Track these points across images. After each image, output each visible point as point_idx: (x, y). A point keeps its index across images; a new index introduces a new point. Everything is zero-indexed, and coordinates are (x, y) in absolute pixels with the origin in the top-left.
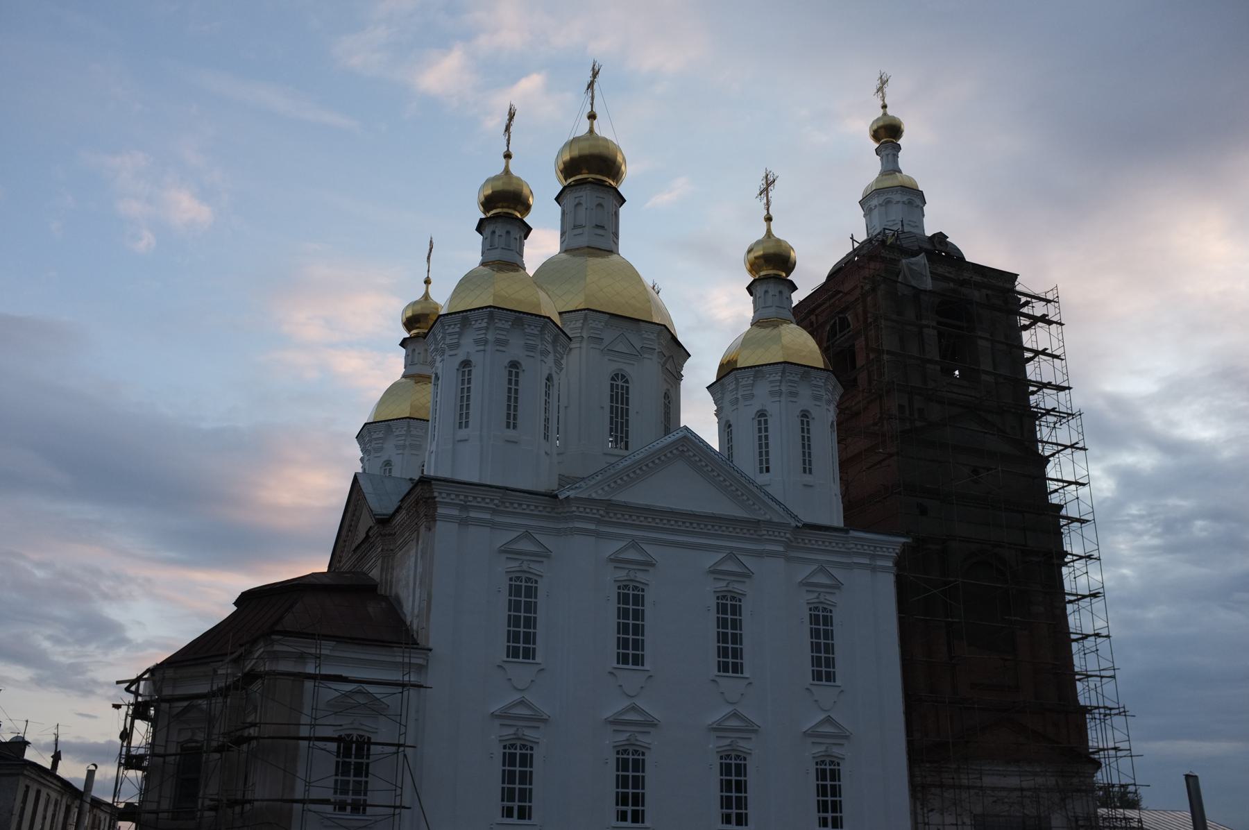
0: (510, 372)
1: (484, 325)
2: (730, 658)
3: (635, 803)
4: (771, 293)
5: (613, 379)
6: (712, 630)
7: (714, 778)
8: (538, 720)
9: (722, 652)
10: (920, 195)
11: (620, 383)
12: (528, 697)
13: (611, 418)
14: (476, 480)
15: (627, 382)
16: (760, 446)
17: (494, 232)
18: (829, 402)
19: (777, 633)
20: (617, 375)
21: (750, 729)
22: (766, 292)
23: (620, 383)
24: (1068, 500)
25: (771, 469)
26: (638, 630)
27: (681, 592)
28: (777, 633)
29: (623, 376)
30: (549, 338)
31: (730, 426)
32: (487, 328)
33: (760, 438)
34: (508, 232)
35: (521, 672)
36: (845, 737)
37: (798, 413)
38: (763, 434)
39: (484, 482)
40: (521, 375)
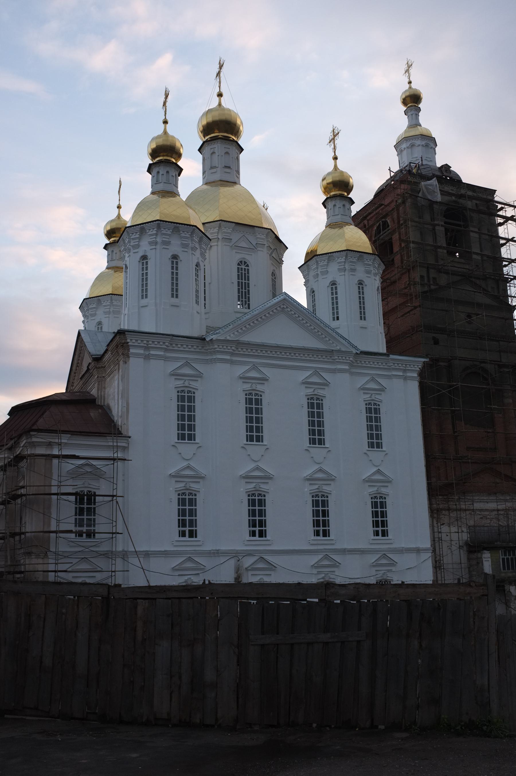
3: (261, 525)
5: (239, 264)
6: (242, 415)
8: (199, 477)
9: (249, 429)
10: (433, 140)
11: (243, 267)
12: (192, 464)
13: (239, 289)
14: (153, 331)
15: (248, 266)
16: (333, 303)
19: (344, 420)
20: (241, 262)
21: (330, 479)
22: (335, 205)
23: (243, 267)
26: (191, 418)
27: (285, 395)
28: (344, 420)
29: (245, 263)
30: (196, 239)
33: (333, 298)
35: (187, 449)
38: (334, 296)
39: (159, 332)
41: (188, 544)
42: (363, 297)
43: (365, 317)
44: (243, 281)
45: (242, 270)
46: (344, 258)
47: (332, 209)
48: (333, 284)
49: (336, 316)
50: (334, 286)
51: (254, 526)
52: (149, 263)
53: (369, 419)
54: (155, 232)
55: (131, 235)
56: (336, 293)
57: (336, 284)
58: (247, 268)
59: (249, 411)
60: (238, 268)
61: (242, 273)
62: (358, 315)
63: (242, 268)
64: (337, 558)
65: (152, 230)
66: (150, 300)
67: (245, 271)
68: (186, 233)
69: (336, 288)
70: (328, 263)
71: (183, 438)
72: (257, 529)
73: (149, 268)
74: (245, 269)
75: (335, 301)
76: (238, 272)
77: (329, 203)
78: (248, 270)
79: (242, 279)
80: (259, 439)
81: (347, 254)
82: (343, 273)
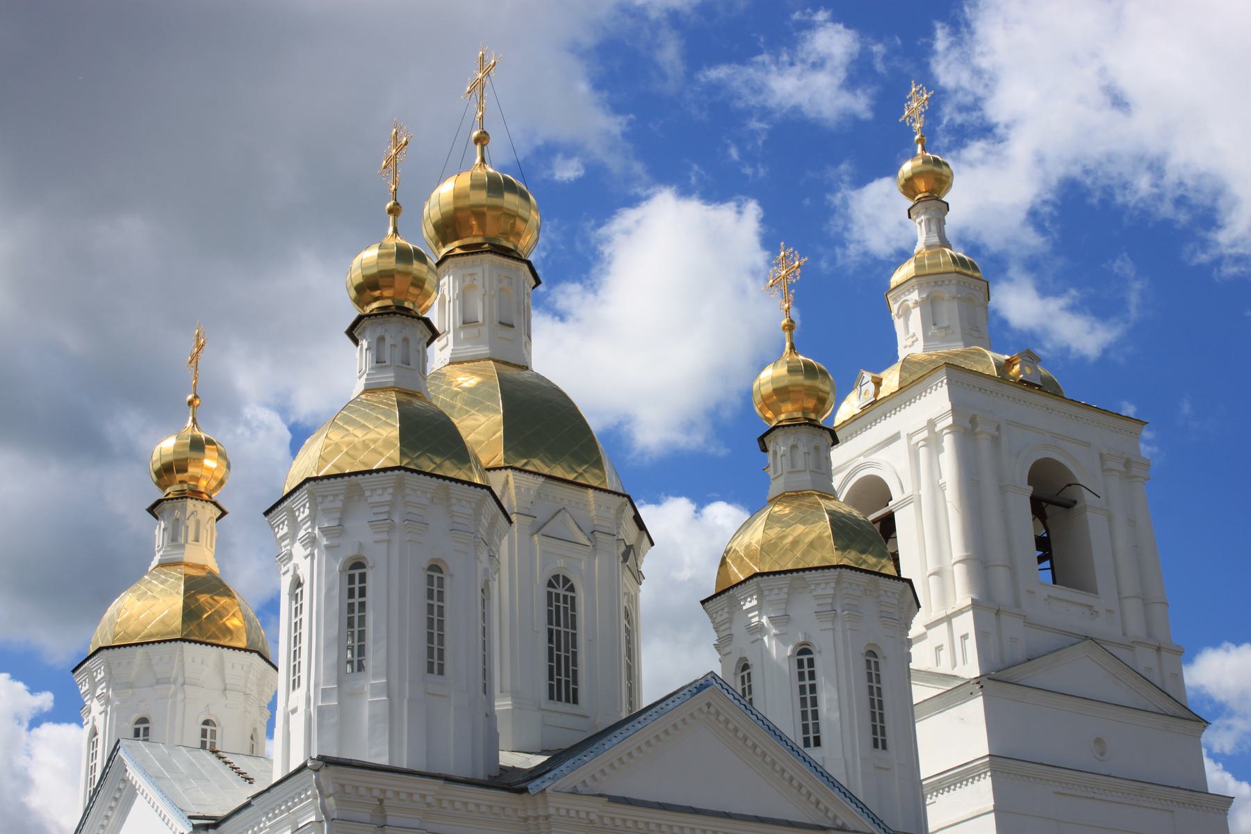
0: (430, 578)
1: (387, 497)
4: (802, 449)
5: (550, 584)
11: (561, 591)
13: (551, 650)
14: (384, 761)
15: (572, 589)
16: (803, 701)
17: (381, 339)
18: (388, 415)
20: (556, 577)
22: (794, 447)
23: (561, 591)
24: (439, 216)
25: (823, 740)
29: (566, 580)
31: (746, 667)
32: (391, 504)
33: (802, 689)
34: (406, 340)
37: (863, 650)
38: (807, 682)
39: (396, 765)
40: (447, 581)
42: (441, 608)
43: (884, 742)
44: (562, 629)
45: (558, 600)
46: (833, 585)
47: (788, 454)
48: (358, 564)
49: (811, 735)
50: (357, 572)
52: (817, 662)
54: (388, 498)
55: (319, 499)
56: (363, 593)
57: (810, 652)
58: (569, 594)
60: (550, 594)
61: (558, 608)
62: (869, 738)
63: (558, 595)
65: (379, 492)
66: (372, 683)
67: (565, 602)
68: (464, 503)
69: (363, 578)
70: (788, 594)
73: (369, 592)
74: (565, 597)
75: (808, 695)
76: (550, 604)
77: (780, 440)
78: (573, 599)
79: (558, 624)
81: (840, 575)
82: (384, 536)
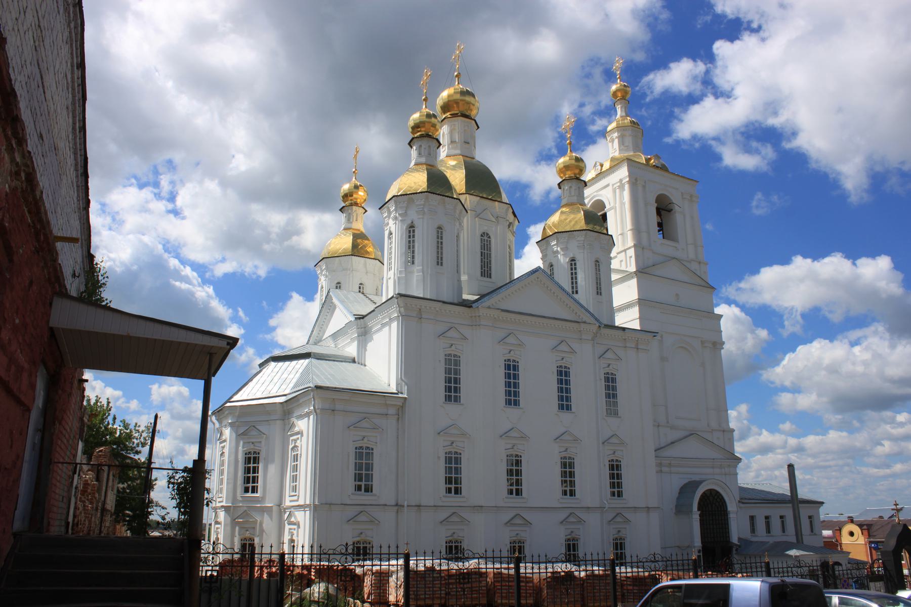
2: (565, 403)
3: (517, 475)
7: (558, 470)
11: (486, 238)
19: (538, 384)
23: (486, 238)
28: (538, 384)
36: (524, 437)
41: (515, 501)
51: (512, 485)
53: (560, 382)
59: (508, 376)
64: (528, 516)
71: (450, 400)
72: (453, 486)
80: (457, 400)
